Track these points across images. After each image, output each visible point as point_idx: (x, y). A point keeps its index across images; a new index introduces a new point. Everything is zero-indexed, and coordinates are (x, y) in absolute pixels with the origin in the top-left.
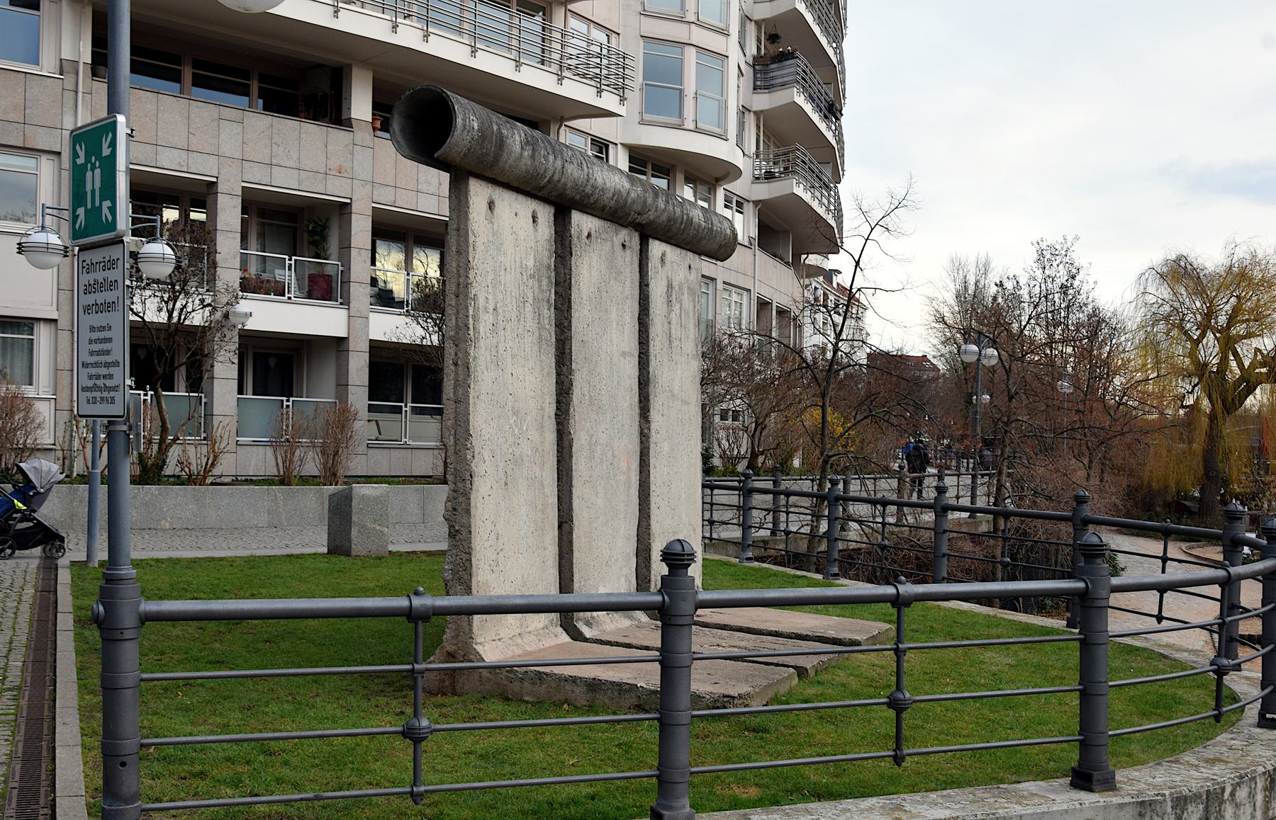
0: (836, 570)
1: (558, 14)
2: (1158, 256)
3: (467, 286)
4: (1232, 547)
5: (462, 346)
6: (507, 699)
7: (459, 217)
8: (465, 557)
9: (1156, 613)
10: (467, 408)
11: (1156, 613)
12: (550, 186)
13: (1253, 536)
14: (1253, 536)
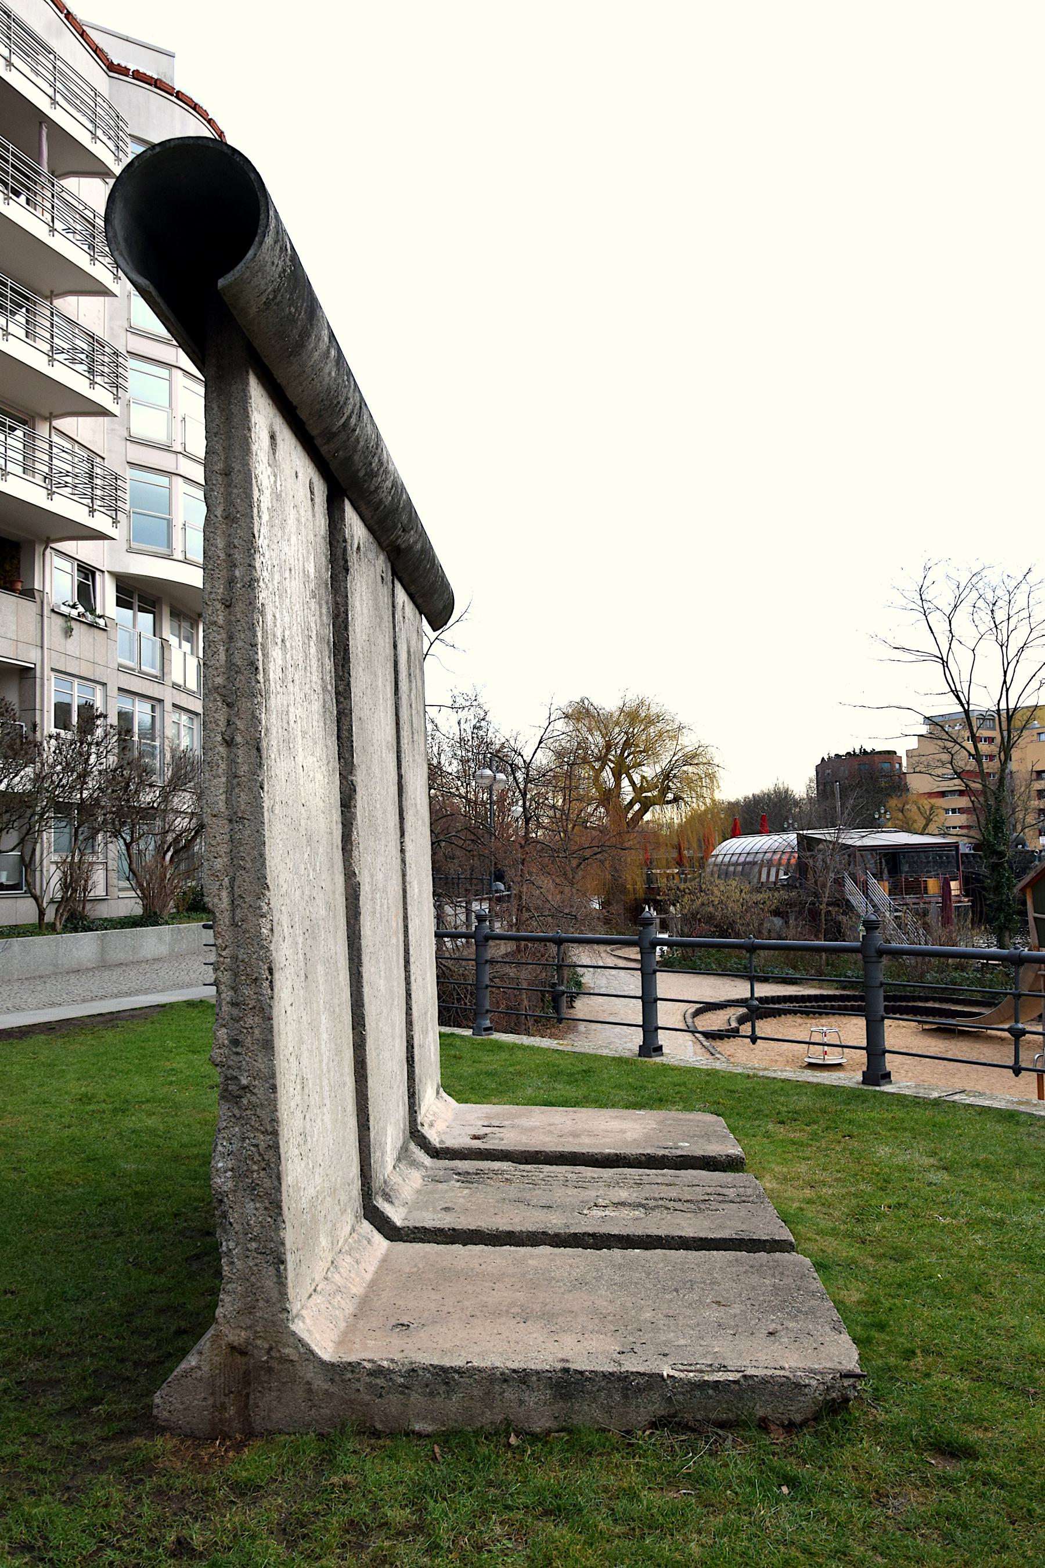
0: (487, 1023)
1: (43, 429)
2: (566, 698)
3: (251, 584)
4: (647, 948)
5: (244, 704)
6: (376, 1434)
7: (228, 449)
8: (262, 1140)
9: (1011, 1063)
10: (259, 832)
11: (1011, 1063)
12: (343, 436)
13: (665, 936)
14: (665, 936)
